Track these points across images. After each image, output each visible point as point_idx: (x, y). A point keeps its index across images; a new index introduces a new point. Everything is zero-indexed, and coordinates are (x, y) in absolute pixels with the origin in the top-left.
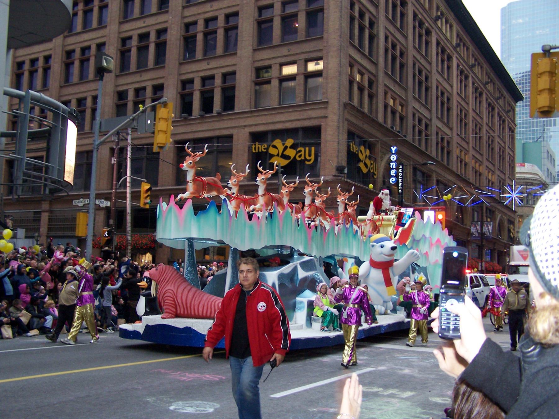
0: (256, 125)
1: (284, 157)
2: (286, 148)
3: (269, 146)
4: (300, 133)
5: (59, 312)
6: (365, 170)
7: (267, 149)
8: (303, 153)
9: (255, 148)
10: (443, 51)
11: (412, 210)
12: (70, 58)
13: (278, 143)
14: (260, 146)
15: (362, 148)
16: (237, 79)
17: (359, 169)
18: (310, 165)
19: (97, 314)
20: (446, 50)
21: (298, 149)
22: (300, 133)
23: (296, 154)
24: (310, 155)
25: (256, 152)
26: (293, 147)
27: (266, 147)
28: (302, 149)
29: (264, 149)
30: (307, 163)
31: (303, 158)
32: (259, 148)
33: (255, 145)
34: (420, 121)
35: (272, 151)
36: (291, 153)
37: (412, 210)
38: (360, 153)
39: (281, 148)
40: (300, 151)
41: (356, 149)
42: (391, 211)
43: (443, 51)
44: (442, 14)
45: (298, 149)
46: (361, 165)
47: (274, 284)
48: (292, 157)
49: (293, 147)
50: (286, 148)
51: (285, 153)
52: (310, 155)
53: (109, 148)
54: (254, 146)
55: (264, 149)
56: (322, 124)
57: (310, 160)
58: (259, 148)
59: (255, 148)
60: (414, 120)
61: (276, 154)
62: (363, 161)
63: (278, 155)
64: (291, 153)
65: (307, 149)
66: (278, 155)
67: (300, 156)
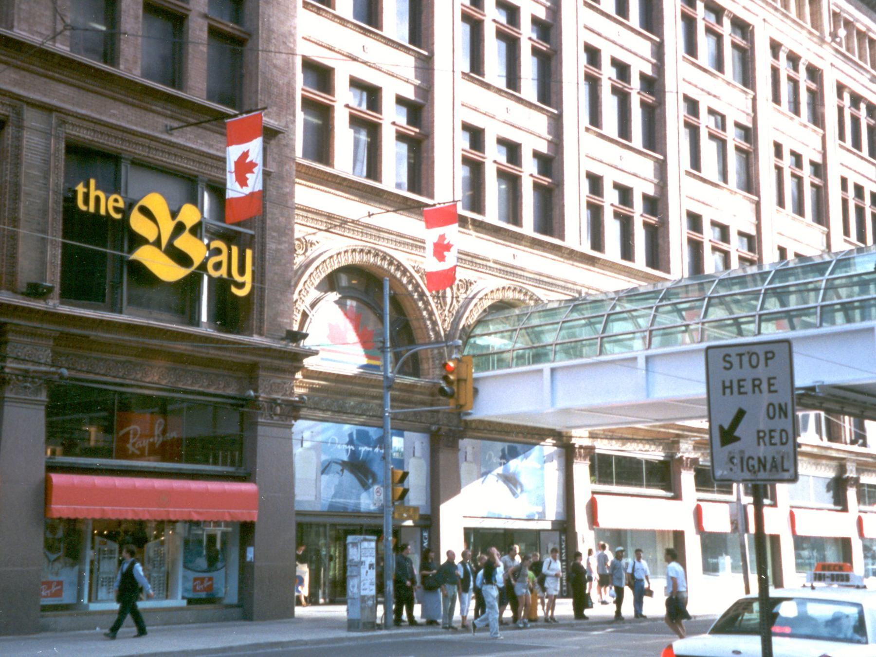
3: (130, 206)
29: (117, 210)
32: (98, 199)
35: (138, 223)
55: (117, 210)
65: (297, 211)
66: (157, 243)
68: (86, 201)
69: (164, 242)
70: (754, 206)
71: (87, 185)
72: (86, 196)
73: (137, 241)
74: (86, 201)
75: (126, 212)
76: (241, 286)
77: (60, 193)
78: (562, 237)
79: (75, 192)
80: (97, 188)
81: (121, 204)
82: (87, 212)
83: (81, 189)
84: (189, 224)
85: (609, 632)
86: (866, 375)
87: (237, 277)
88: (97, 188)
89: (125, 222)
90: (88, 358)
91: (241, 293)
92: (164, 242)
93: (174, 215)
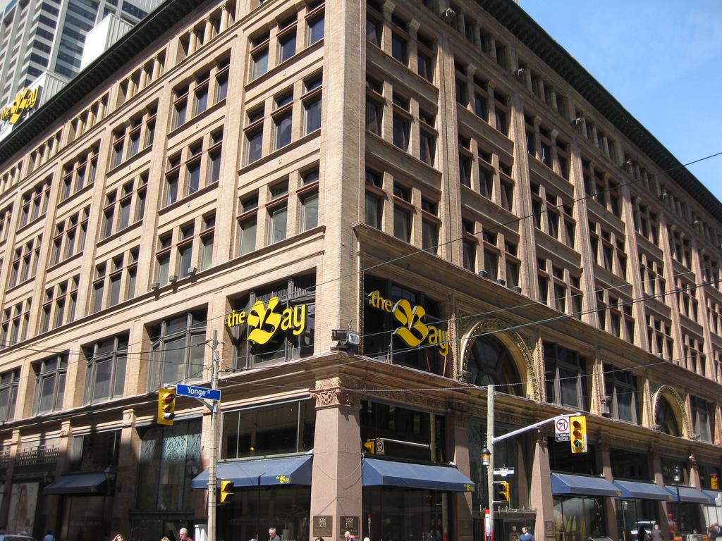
0: (235, 283)
1: (267, 328)
4: (291, 285)
6: (412, 341)
7: (245, 319)
8: (290, 317)
9: (231, 319)
11: (338, 403)
12: (44, 444)
14: (237, 315)
15: (405, 304)
21: (284, 313)
22: (291, 285)
23: (282, 319)
24: (299, 319)
26: (279, 309)
27: (244, 316)
29: (242, 319)
30: (295, 333)
31: (290, 326)
35: (252, 321)
36: (275, 320)
37: (338, 403)
39: (262, 313)
40: (287, 315)
42: (202, 396)
46: (404, 333)
49: (279, 309)
51: (267, 322)
52: (299, 319)
53: (143, 324)
55: (242, 319)
56: (318, 264)
59: (231, 319)
62: (407, 326)
63: (258, 327)
64: (275, 320)
66: (258, 327)
67: (286, 324)
68: (299, 311)
73: (399, 324)
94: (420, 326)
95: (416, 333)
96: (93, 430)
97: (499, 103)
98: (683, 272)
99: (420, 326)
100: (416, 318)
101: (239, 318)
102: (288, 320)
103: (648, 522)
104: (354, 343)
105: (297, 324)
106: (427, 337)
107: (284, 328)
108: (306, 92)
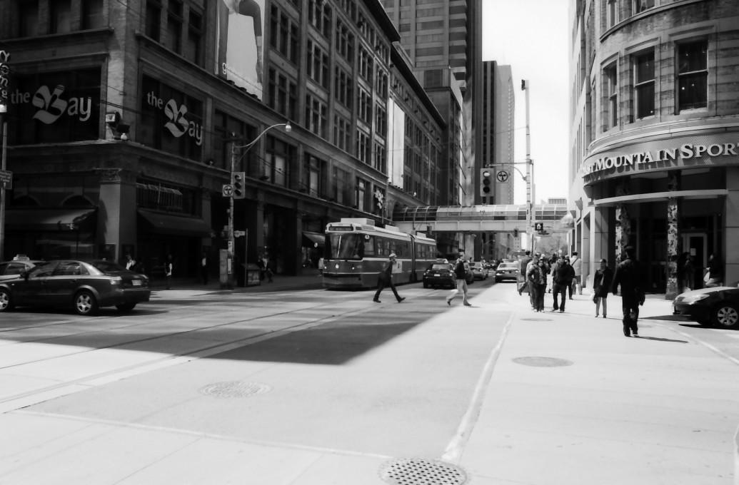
2: (54, 98)
3: (32, 96)
5: (146, 275)
7: (30, 99)
8: (76, 105)
9: (15, 97)
10: (344, 30)
13: (44, 90)
14: (21, 94)
15: (172, 103)
16: (109, 70)
17: (378, 207)
18: (88, 120)
19: (692, 296)
20: (367, 53)
21: (71, 100)
25: (16, 104)
26: (64, 97)
28: (76, 100)
29: (27, 99)
30: (81, 119)
31: (76, 112)
32: (19, 97)
33: (15, 93)
34: (342, 122)
35: (37, 102)
36: (61, 105)
38: (166, 108)
40: (74, 102)
41: (159, 102)
43: (344, 30)
44: (364, 20)
45: (71, 100)
47: (35, 264)
48: (63, 110)
50: (54, 98)
52: (85, 109)
54: (13, 95)
55: (160, 105)
57: (85, 116)
58: (19, 97)
59: (15, 97)
60: (336, 122)
61: (41, 107)
64: (61, 105)
65: (82, 100)
66: (44, 108)
67: (73, 110)
68: (15, 100)
69: (175, 120)
70: (526, 86)
71: (151, 94)
72: (151, 98)
73: (167, 119)
74: (15, 100)
75: (163, 106)
76: (199, 141)
77: (391, 97)
78: (328, 140)
79: (147, 97)
80: (19, 92)
81: (162, 103)
82: (151, 105)
83: (149, 95)
84: (183, 114)
85: (709, 349)
86: (731, 336)
87: (198, 138)
88: (19, 92)
89: (163, 110)
90: (419, 198)
91: (199, 144)
92: (175, 120)
93: (178, 109)
94: (183, 121)
95: (180, 127)
96: (77, 244)
97: (318, 7)
98: (378, 94)
99: (183, 121)
100: (180, 114)
101: (24, 98)
102: (74, 108)
103: (428, 260)
104: (657, 98)
105: (83, 113)
106: (188, 130)
107: (70, 114)
108: (642, 35)
